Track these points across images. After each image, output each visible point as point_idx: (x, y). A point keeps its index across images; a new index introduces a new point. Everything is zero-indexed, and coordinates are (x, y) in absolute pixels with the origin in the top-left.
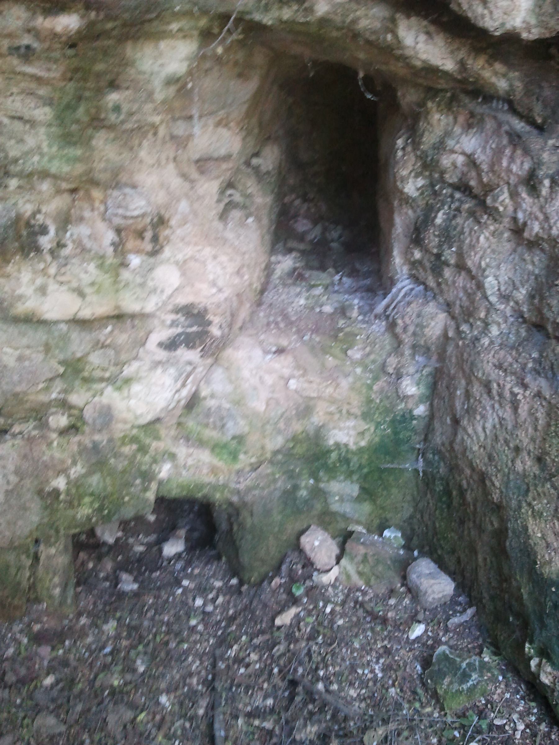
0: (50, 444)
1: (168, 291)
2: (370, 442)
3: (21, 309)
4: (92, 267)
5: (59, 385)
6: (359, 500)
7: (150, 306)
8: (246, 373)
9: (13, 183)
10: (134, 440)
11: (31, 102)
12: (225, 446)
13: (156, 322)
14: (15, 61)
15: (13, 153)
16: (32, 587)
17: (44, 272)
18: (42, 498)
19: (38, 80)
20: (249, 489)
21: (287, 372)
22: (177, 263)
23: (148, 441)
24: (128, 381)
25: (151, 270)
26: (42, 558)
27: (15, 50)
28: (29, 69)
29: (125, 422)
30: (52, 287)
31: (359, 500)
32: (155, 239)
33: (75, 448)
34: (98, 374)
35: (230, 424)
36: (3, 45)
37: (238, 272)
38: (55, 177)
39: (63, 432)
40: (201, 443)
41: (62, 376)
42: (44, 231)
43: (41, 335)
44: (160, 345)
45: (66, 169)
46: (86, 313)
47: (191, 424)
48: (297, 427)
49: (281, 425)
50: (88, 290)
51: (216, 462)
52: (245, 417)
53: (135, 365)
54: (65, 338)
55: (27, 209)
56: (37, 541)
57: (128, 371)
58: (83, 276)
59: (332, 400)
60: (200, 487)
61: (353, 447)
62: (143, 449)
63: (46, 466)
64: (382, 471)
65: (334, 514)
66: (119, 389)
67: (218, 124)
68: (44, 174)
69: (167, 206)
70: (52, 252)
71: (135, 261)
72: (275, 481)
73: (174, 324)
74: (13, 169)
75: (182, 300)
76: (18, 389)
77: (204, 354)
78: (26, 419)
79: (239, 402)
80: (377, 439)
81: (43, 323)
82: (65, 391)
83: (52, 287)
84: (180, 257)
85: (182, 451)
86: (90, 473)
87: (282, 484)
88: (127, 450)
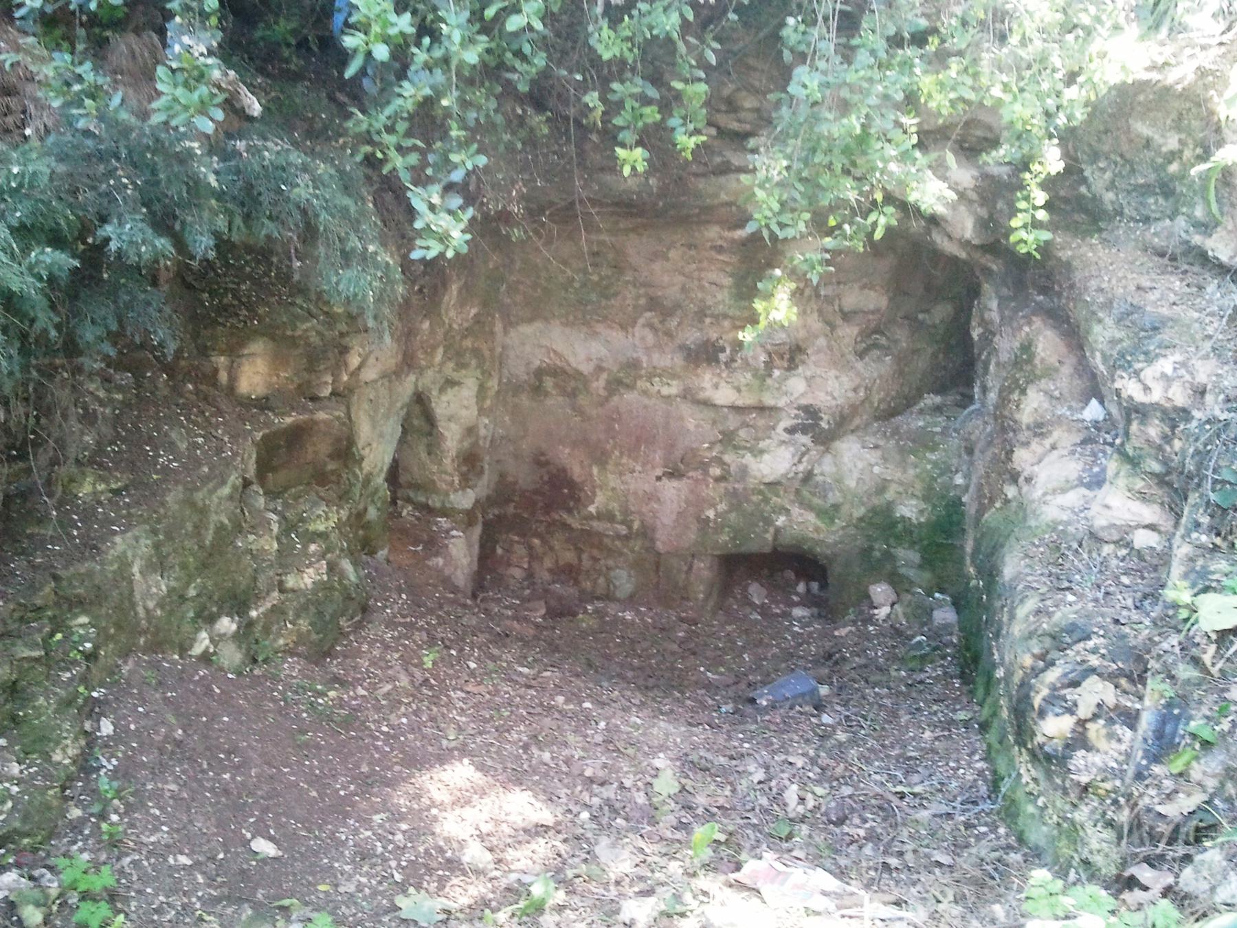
0: (707, 486)
1: (796, 395)
2: (928, 520)
3: (702, 396)
4: (749, 376)
5: (718, 448)
6: (920, 567)
7: (781, 403)
8: (846, 459)
9: (708, 320)
10: (760, 492)
11: (722, 275)
12: (826, 512)
13: (784, 414)
14: (713, 253)
15: (709, 303)
16: (685, 588)
17: (719, 375)
18: (699, 522)
19: (727, 263)
20: (836, 543)
21: (873, 461)
22: (806, 378)
23: (769, 495)
24: (762, 452)
25: (786, 379)
26: (695, 567)
27: (714, 248)
28: (721, 257)
29: (755, 478)
30: (723, 384)
31: (920, 567)
32: (792, 360)
33: (723, 491)
34: (743, 443)
35: (830, 495)
36: (462, 303)
37: (855, 390)
38: (732, 318)
39: (718, 480)
40: (810, 507)
41: (720, 441)
42: (723, 350)
43: (710, 414)
44: (786, 430)
45: (738, 313)
46: (740, 403)
47: (805, 493)
48: (876, 501)
49: (865, 499)
50: (743, 389)
51: (819, 523)
52: (841, 491)
53: (768, 441)
54: (726, 418)
55: (714, 336)
56: (693, 556)
57: (762, 445)
58: (742, 380)
59: (901, 483)
60: (805, 539)
61: (915, 522)
62: (766, 500)
63: (704, 501)
64: (939, 545)
65: (900, 576)
66: (755, 456)
67: (863, 287)
68: (725, 316)
69: (806, 339)
70: (726, 364)
71: (777, 373)
72: (856, 539)
73: (796, 417)
74: (708, 312)
75: (804, 402)
76: (694, 446)
77: (816, 441)
78: (696, 469)
79: (839, 481)
80: (934, 518)
81: (715, 406)
82: (722, 453)
83: (723, 384)
84: (808, 373)
85: (796, 510)
86: (730, 511)
87: (861, 542)
88: (755, 498)
